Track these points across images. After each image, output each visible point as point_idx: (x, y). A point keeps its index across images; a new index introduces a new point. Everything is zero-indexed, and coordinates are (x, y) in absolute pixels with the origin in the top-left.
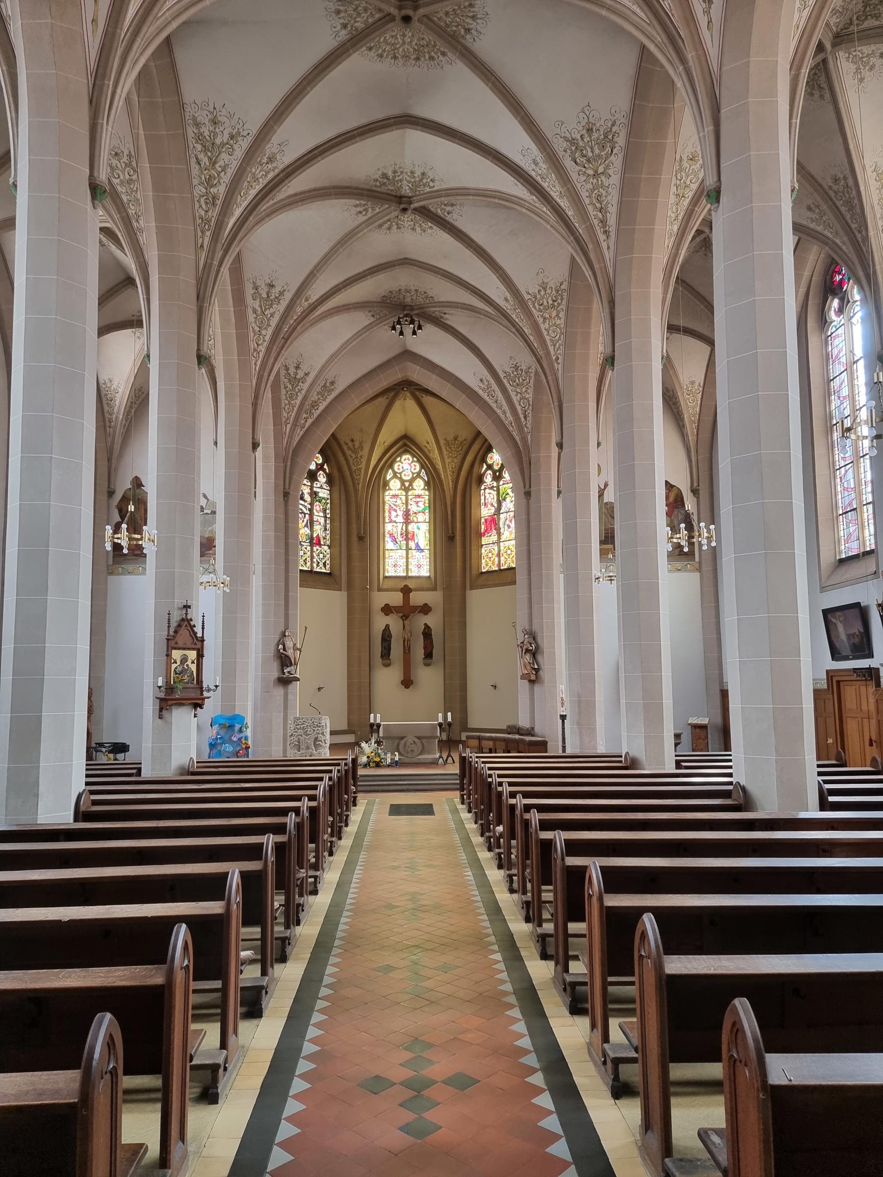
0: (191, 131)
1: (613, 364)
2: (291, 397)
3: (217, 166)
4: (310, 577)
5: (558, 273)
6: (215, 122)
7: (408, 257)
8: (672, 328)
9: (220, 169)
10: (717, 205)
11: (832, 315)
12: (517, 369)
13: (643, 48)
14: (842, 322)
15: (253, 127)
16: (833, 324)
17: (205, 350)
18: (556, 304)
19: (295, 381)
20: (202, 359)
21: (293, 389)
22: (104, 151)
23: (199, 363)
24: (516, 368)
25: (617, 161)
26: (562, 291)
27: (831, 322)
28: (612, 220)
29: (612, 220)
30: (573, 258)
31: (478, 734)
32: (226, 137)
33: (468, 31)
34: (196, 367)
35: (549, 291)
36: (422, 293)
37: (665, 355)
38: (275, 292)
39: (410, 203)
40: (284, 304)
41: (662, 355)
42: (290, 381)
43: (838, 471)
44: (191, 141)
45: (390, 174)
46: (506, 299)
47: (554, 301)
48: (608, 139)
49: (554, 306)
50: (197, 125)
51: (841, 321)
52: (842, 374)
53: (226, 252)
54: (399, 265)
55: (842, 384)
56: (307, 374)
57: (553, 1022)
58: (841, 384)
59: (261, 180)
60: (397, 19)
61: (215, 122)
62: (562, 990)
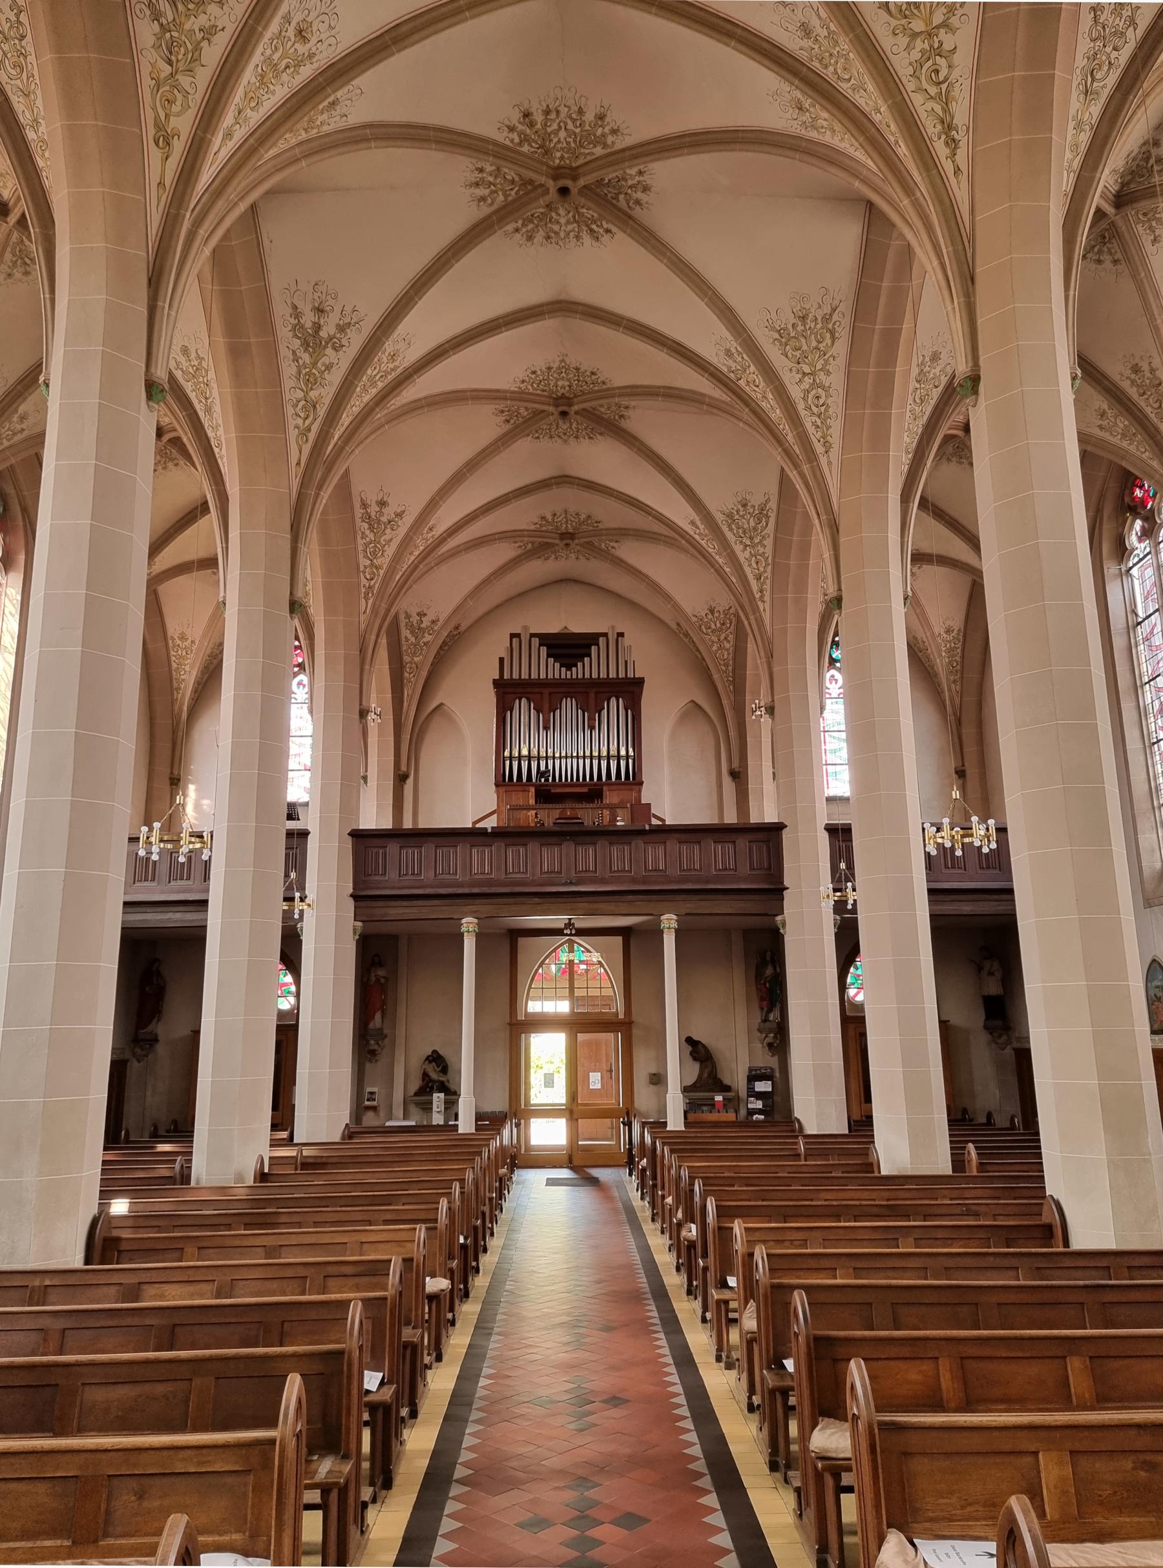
0: (359, 512)
1: (840, 607)
2: (374, 554)
3: (319, 365)
4: (849, 1469)
5: (765, 489)
6: (320, 310)
7: (568, 473)
8: (919, 558)
9: (323, 369)
10: (974, 397)
11: (1133, 540)
12: (803, 318)
13: (870, 205)
14: (1148, 550)
15: (371, 318)
16: (1135, 552)
17: (299, 594)
18: (724, 627)
19: (418, 631)
20: (296, 606)
21: (314, 364)
22: (167, 323)
23: (292, 611)
24: (712, 611)
25: (841, 349)
26: (834, 324)
27: (1133, 550)
28: (961, 114)
29: (961, 114)
30: (783, 469)
31: (996, 1223)
32: (332, 331)
33: (622, 416)
34: (288, 615)
35: (716, 615)
36: (588, 373)
37: (910, 594)
38: (389, 513)
39: (575, 179)
40: (402, 531)
41: (905, 592)
42: (412, 633)
43: (1156, 746)
44: (358, 521)
45: (550, 518)
46: (693, 523)
47: (819, 342)
48: (762, 513)
49: (722, 629)
50: (364, 505)
51: (1145, 548)
52: (1153, 617)
53: (329, 470)
54: (549, 312)
55: (1153, 629)
56: (399, 515)
57: (754, 1496)
58: (1152, 632)
59: (379, 383)
60: (551, 191)
61: (320, 310)
62: (783, 1482)
